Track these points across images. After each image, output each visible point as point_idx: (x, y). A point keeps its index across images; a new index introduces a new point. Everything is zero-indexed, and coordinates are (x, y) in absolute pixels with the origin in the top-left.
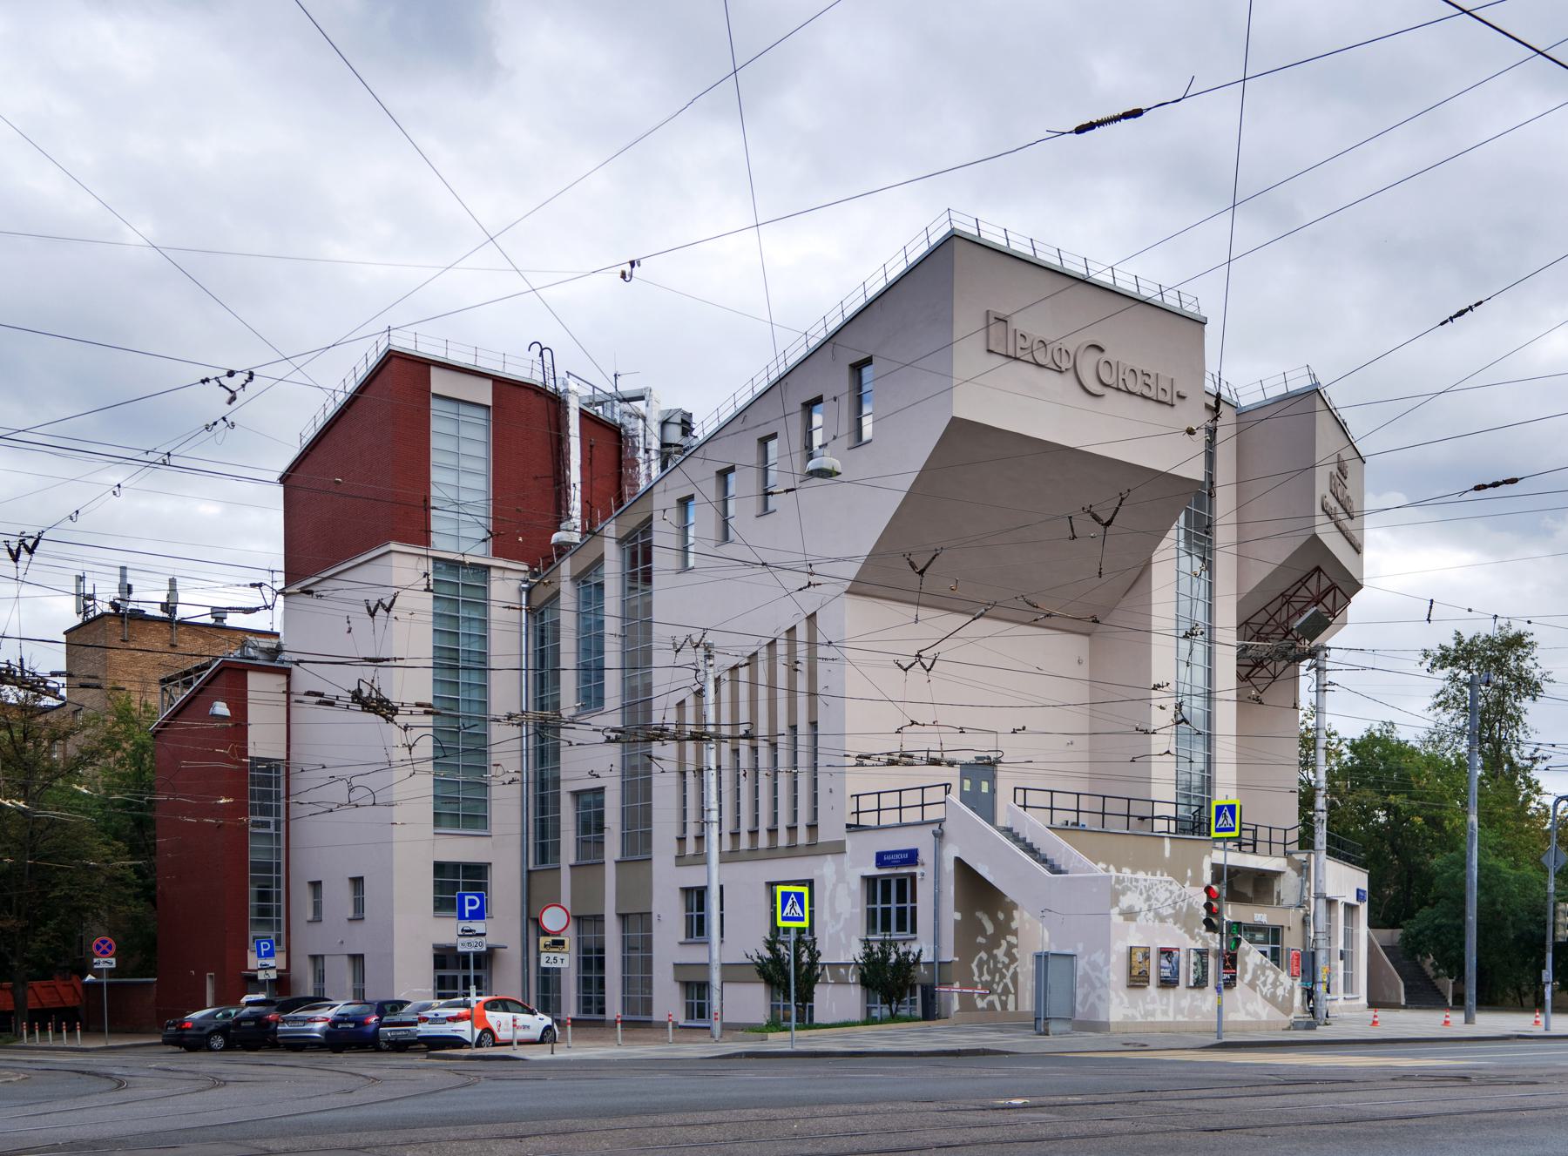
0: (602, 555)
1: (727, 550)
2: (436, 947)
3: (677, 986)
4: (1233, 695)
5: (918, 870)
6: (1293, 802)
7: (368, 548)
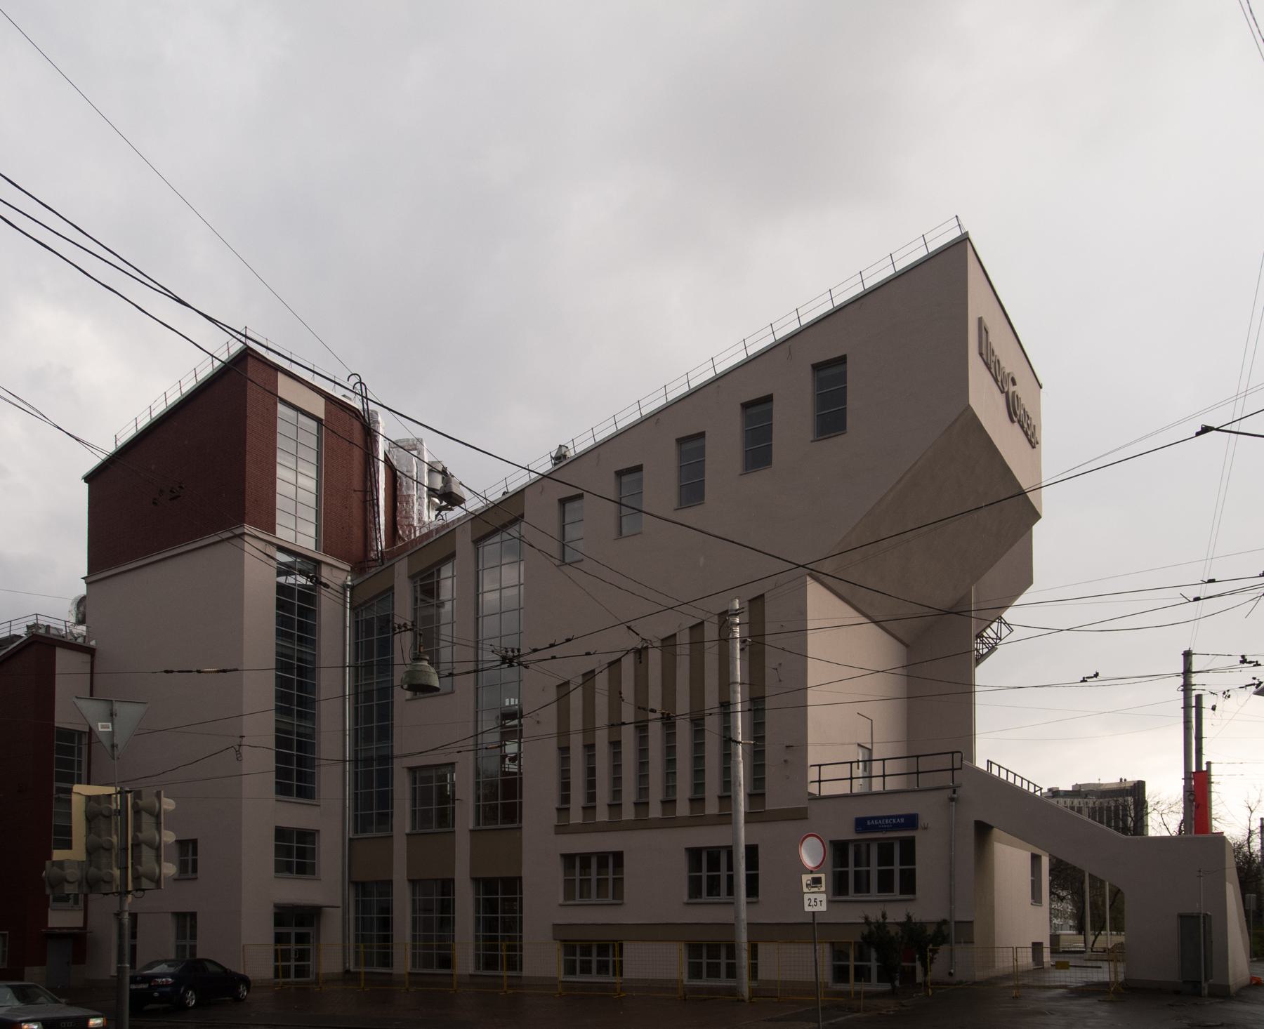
0: (392, 588)
1: (690, 515)
2: (276, 906)
3: (558, 945)
4: (442, 644)
5: (917, 834)
6: (1180, 660)
7: (132, 558)
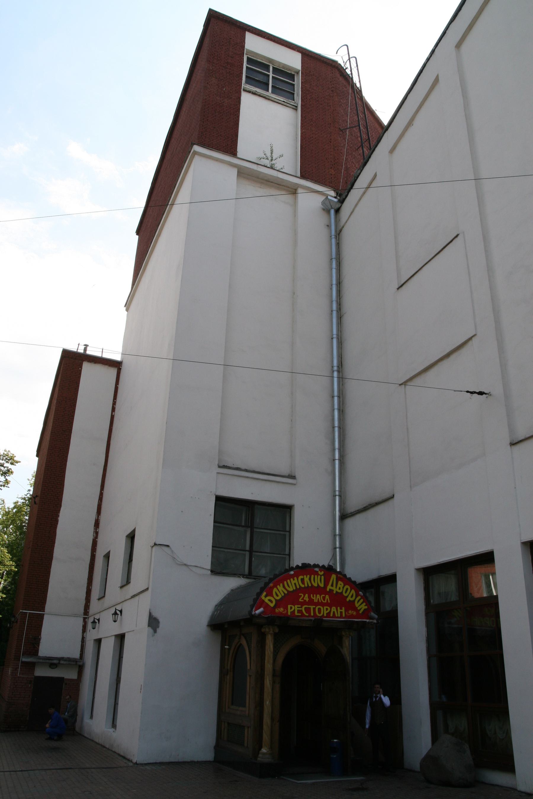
2: (210, 11)
7: (53, 428)
